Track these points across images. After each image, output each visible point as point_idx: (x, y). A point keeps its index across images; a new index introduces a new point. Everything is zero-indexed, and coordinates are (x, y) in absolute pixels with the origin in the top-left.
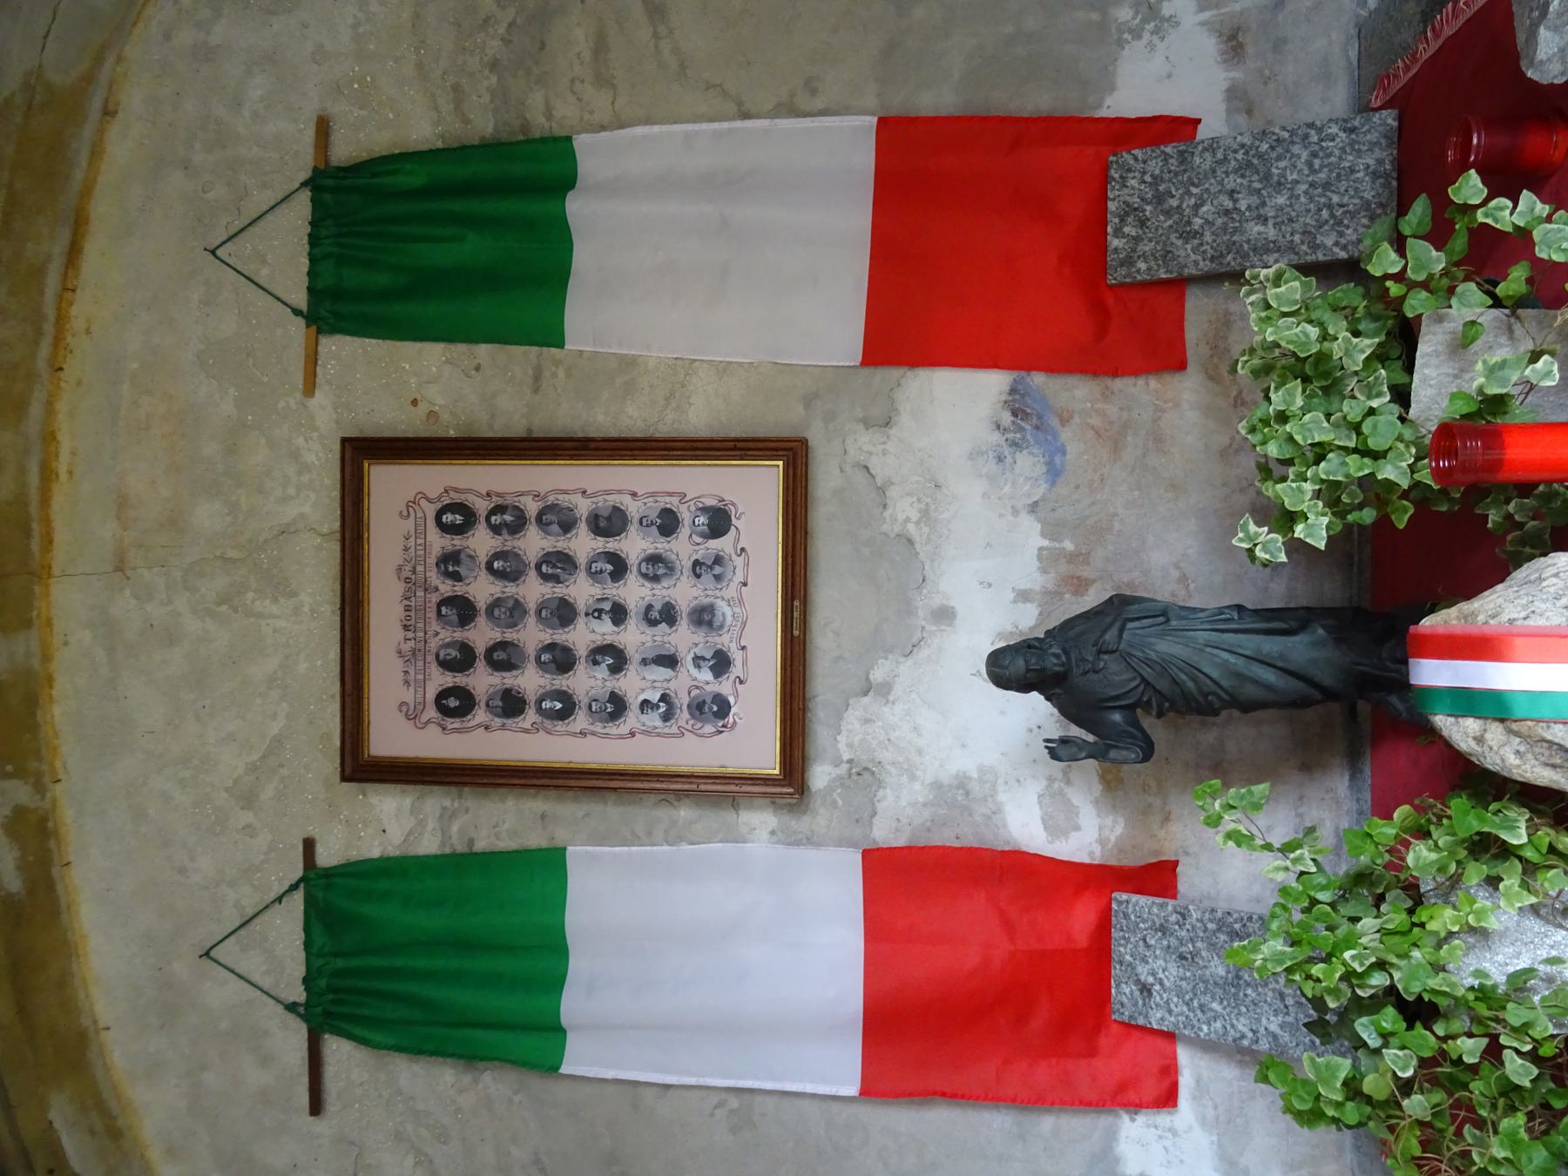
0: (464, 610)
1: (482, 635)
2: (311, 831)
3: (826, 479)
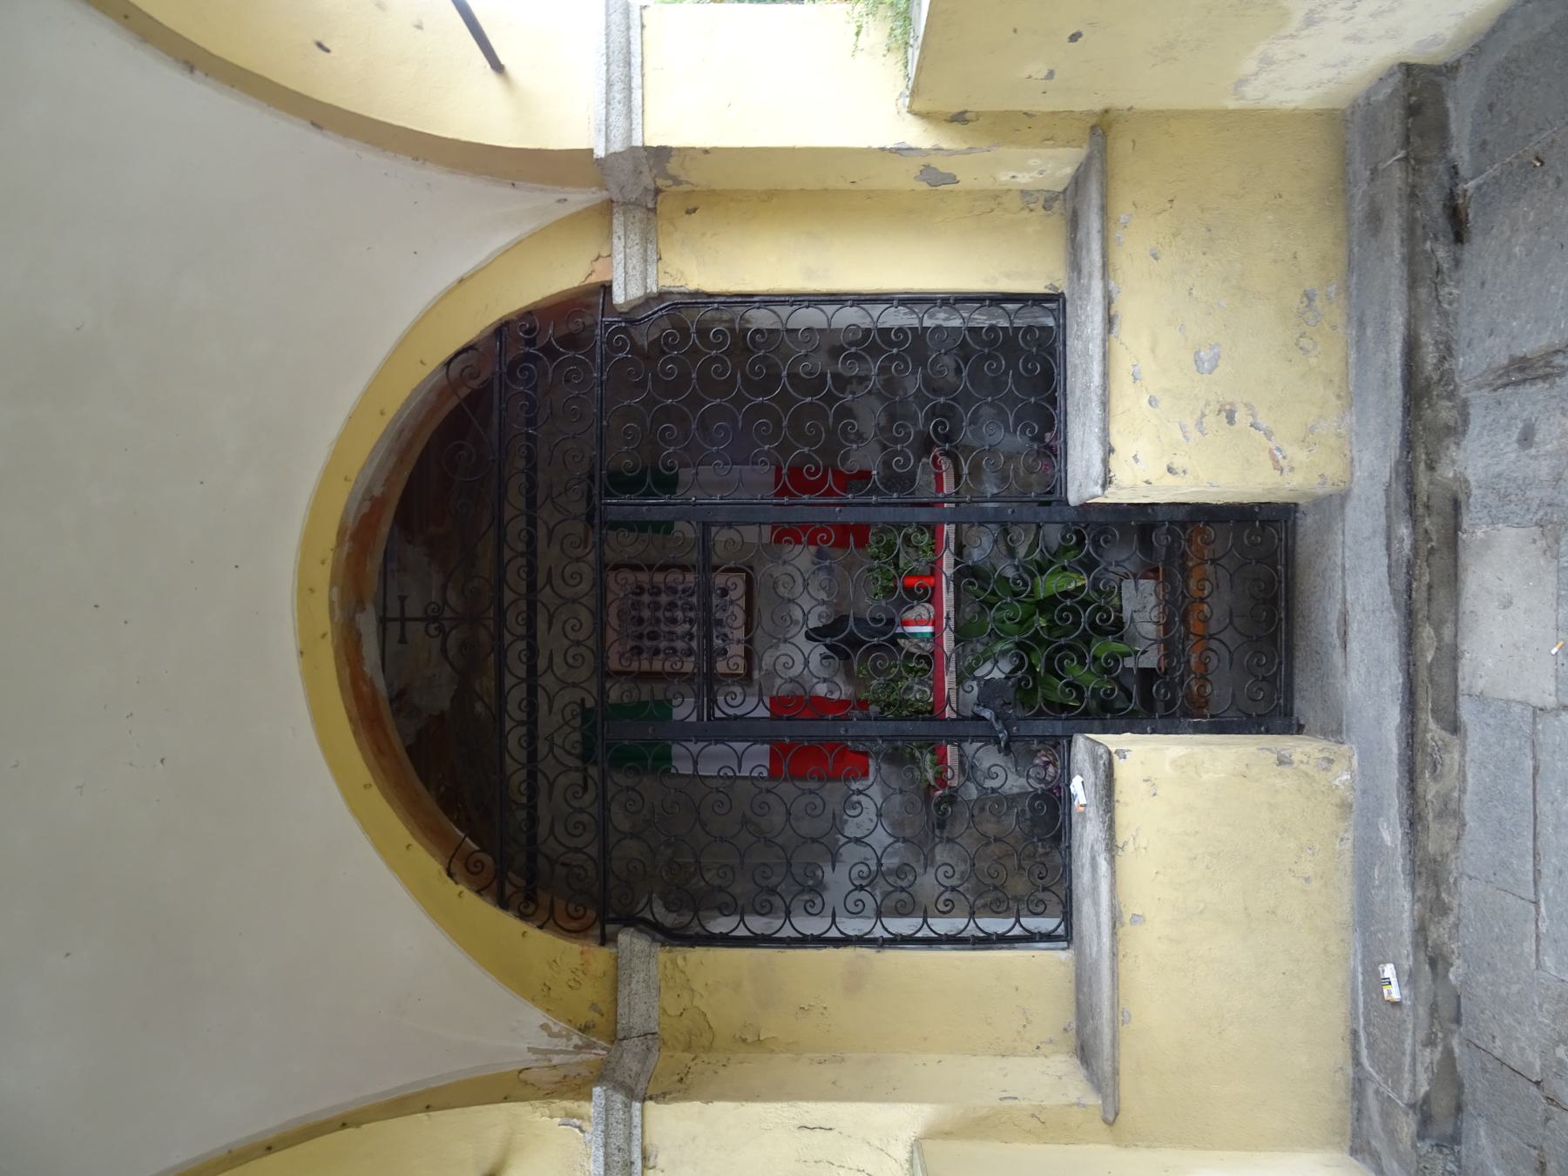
0: (640, 621)
1: (646, 629)
2: (332, 54)
3: (759, 577)
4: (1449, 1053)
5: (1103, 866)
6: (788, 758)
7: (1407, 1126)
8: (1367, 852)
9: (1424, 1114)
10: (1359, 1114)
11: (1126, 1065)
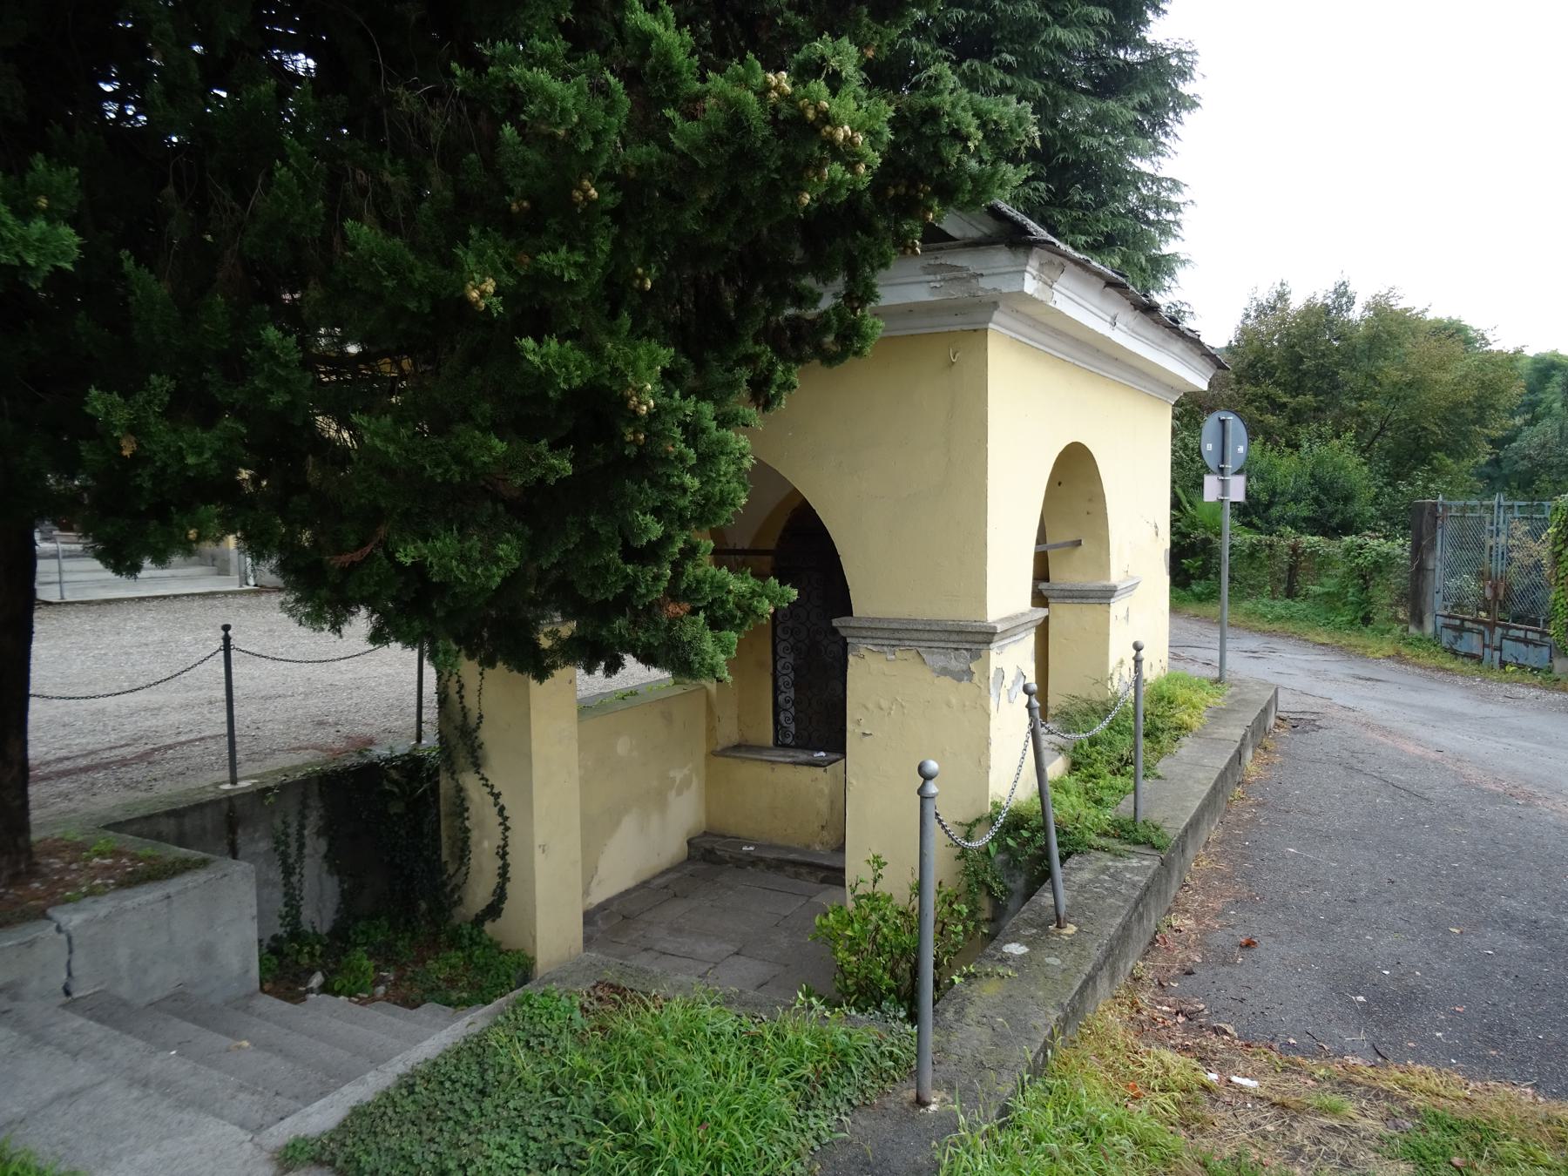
4: (727, 862)
5: (788, 760)
6: (1226, 552)
7: (708, 846)
8: (790, 850)
9: (711, 851)
10: (716, 836)
11: (730, 760)
